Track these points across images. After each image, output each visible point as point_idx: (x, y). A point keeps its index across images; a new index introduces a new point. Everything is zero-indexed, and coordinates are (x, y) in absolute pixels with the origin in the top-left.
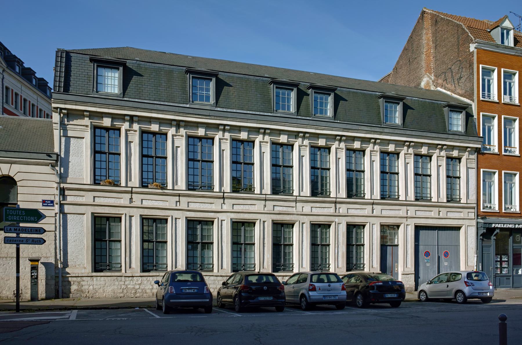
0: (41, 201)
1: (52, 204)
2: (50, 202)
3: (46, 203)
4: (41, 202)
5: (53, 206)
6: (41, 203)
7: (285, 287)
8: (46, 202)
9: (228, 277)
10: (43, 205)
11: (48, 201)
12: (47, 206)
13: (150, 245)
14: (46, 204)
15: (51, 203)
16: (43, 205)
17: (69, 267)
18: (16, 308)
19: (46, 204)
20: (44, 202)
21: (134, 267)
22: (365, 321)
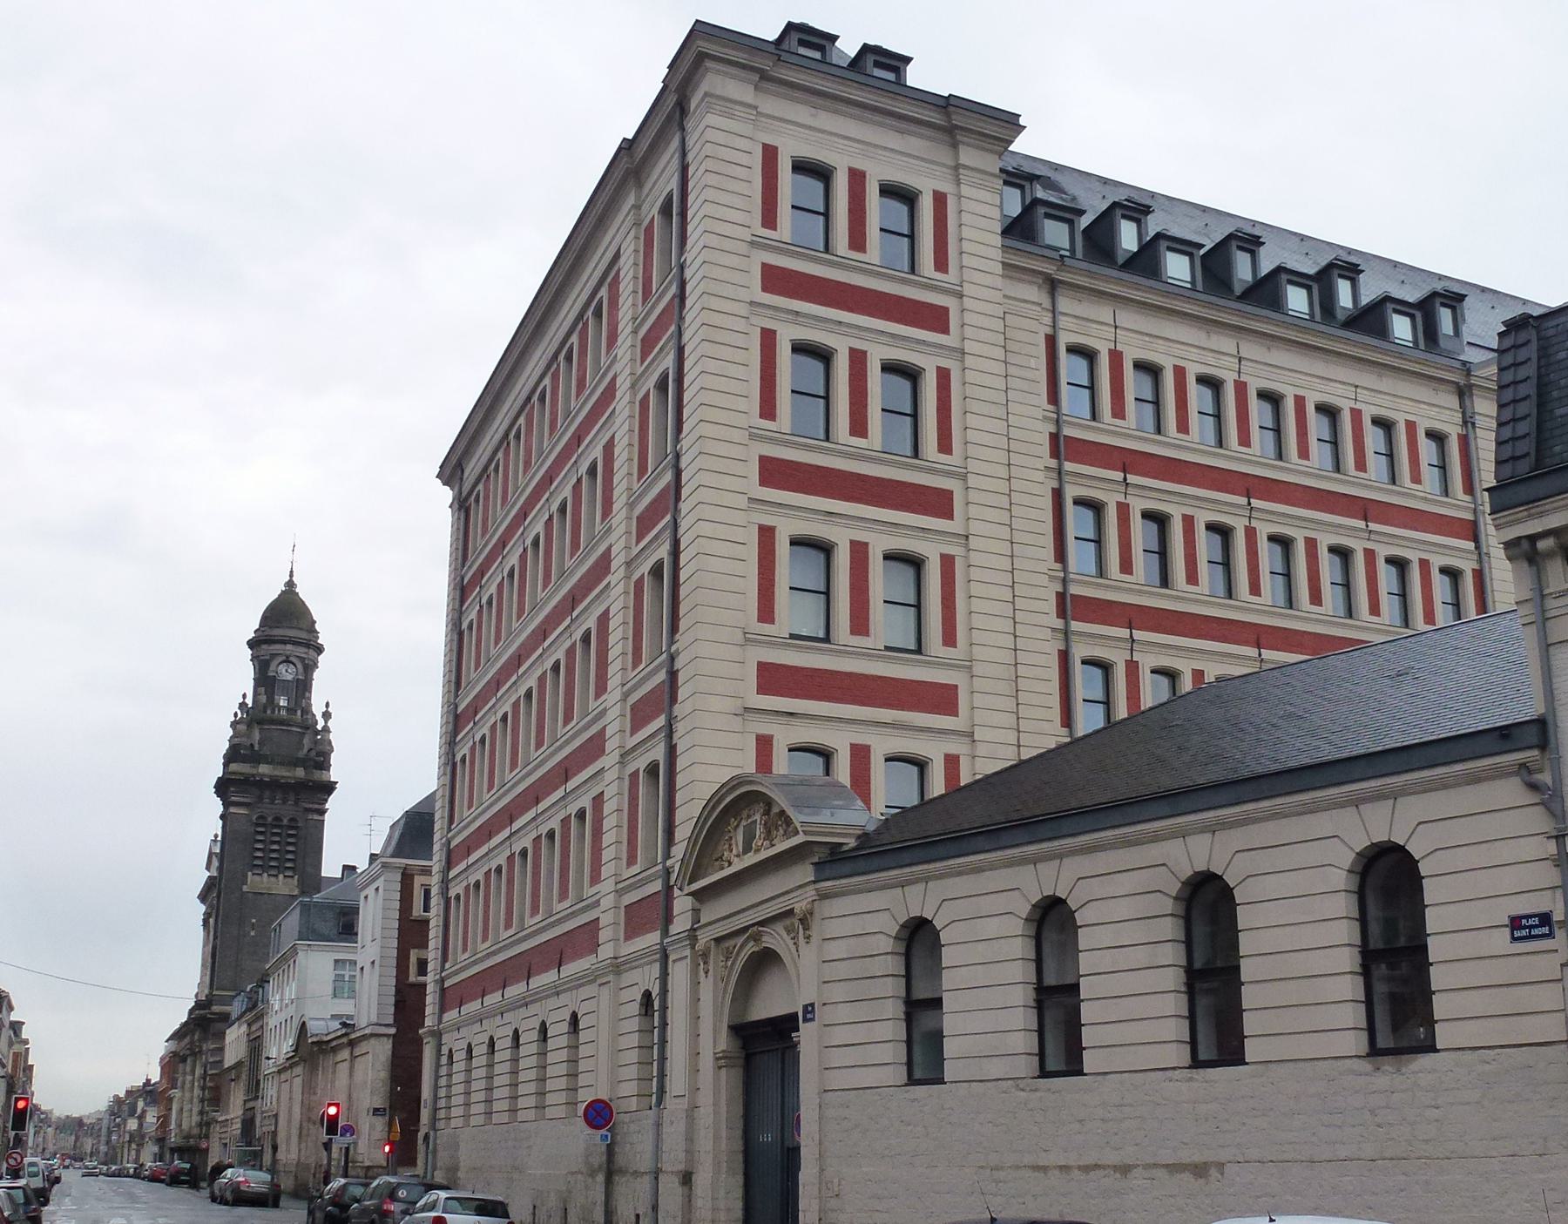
0: (1507, 922)
1: (1545, 930)
2: (1536, 921)
3: (1525, 927)
4: (1506, 926)
5: (1550, 935)
6: (1507, 930)
7: (199, 998)
8: (1524, 922)
9: (686, 841)
10: (1514, 939)
11: (1528, 917)
12: (1530, 937)
13: (1485, 425)
14: (1524, 933)
15: (1541, 925)
16: (1514, 939)
17: (506, 1202)
18: (1191, 1038)
19: (1524, 933)
20: (1515, 923)
21: (817, 858)
22: (558, 994)
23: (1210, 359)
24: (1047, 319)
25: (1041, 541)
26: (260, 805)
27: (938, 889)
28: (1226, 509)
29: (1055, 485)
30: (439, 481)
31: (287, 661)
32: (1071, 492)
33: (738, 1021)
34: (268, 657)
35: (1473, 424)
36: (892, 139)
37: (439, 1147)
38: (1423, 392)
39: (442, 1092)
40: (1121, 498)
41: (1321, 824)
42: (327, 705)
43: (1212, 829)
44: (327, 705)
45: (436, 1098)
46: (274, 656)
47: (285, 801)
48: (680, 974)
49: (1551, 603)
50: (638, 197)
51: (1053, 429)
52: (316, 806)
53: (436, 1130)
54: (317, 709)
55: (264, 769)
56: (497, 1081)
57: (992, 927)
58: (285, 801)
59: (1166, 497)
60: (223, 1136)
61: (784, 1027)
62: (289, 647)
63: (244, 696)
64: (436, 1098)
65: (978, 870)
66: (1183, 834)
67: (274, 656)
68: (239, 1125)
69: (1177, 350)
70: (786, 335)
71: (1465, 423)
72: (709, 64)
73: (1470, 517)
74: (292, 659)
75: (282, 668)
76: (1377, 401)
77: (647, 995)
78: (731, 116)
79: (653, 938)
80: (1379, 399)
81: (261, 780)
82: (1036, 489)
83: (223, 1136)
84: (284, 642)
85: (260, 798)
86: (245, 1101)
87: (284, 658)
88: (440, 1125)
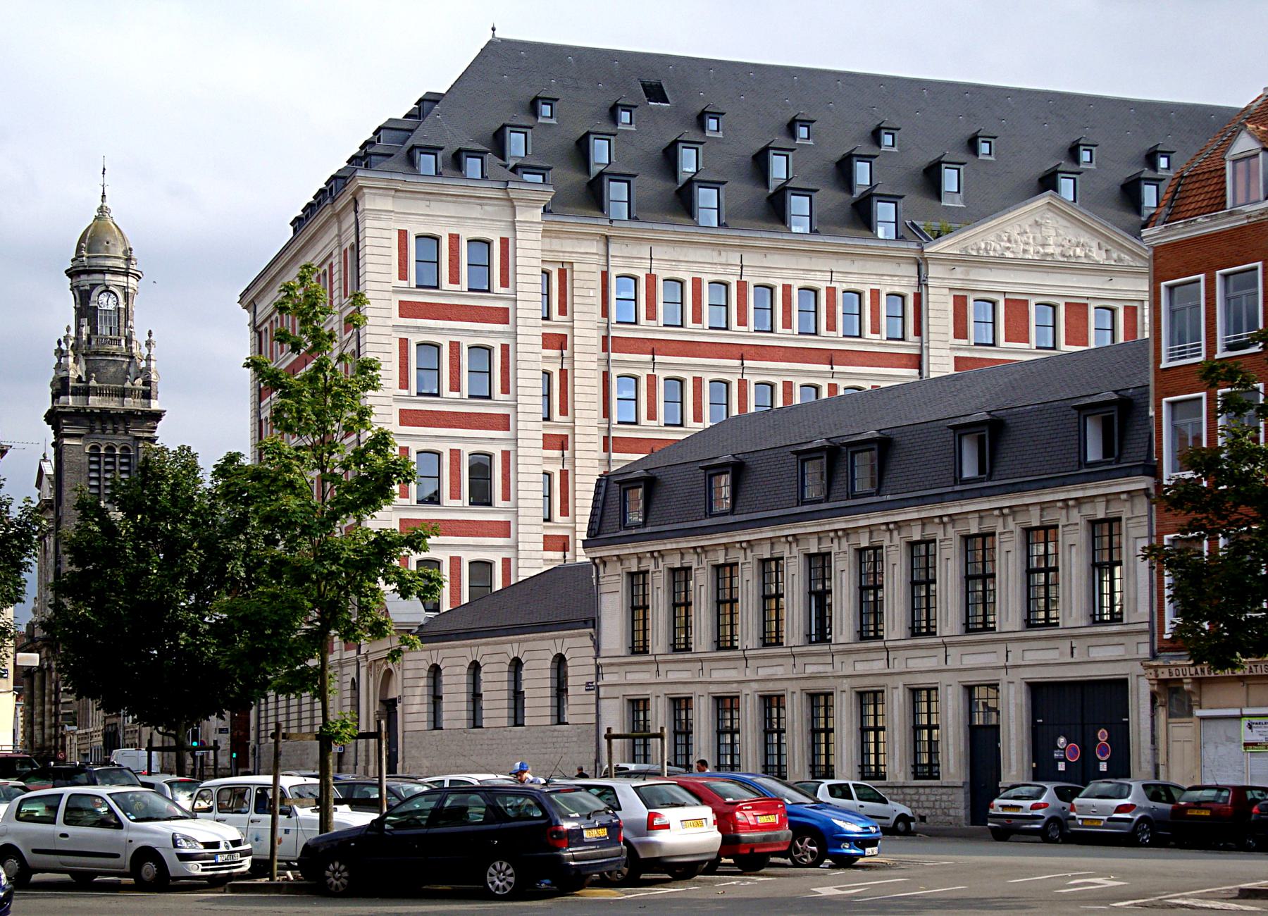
23: (720, 269)
24: (603, 261)
25: (595, 406)
26: (92, 436)
27: (444, 653)
28: (724, 370)
29: (605, 369)
30: (239, 306)
31: (107, 290)
32: (614, 372)
33: (383, 699)
34: (88, 288)
35: (926, 285)
36: (476, 212)
37: (262, 755)
38: (888, 268)
39: (263, 721)
40: (650, 372)
41: (546, 644)
42: (150, 334)
43: (519, 641)
44: (150, 334)
45: (259, 724)
46: (93, 286)
47: (115, 431)
48: (363, 671)
49: (601, 580)
50: (340, 229)
51: (604, 333)
52: (146, 435)
53: (259, 744)
54: (140, 337)
55: (95, 402)
56: (304, 715)
57: (458, 670)
58: (115, 431)
59: (682, 367)
60: (82, 747)
61: (394, 702)
62: (108, 277)
63: (68, 329)
64: (259, 724)
65: (454, 647)
66: (511, 642)
67: (93, 286)
68: (101, 738)
69: (695, 267)
70: (414, 340)
71: (920, 284)
72: (365, 191)
73: (916, 352)
74: (111, 288)
75: (103, 298)
76: (849, 279)
77: (353, 679)
78: (379, 219)
79: (354, 652)
80: (850, 278)
81: (92, 411)
82: (592, 374)
83: (82, 747)
84: (102, 272)
85: (92, 430)
86: (106, 718)
87: (104, 288)
88: (263, 741)
